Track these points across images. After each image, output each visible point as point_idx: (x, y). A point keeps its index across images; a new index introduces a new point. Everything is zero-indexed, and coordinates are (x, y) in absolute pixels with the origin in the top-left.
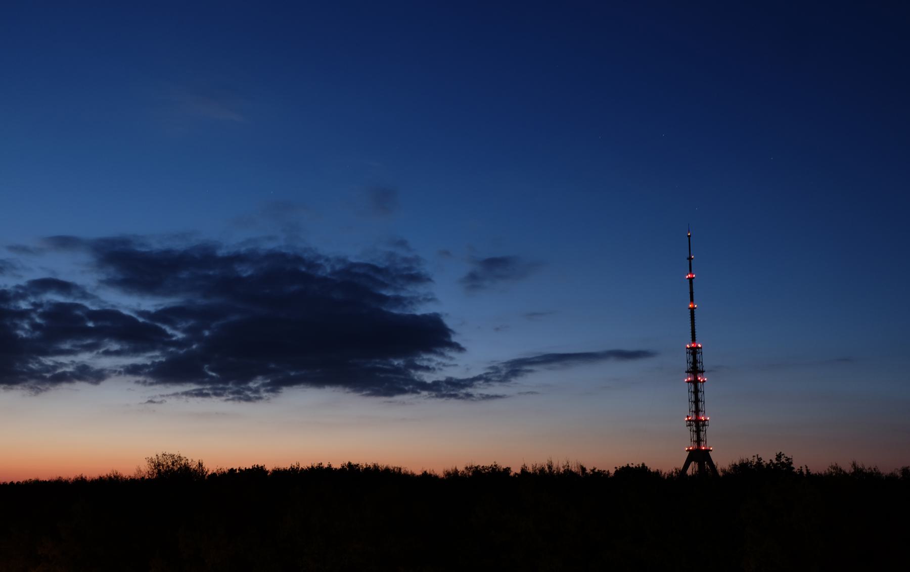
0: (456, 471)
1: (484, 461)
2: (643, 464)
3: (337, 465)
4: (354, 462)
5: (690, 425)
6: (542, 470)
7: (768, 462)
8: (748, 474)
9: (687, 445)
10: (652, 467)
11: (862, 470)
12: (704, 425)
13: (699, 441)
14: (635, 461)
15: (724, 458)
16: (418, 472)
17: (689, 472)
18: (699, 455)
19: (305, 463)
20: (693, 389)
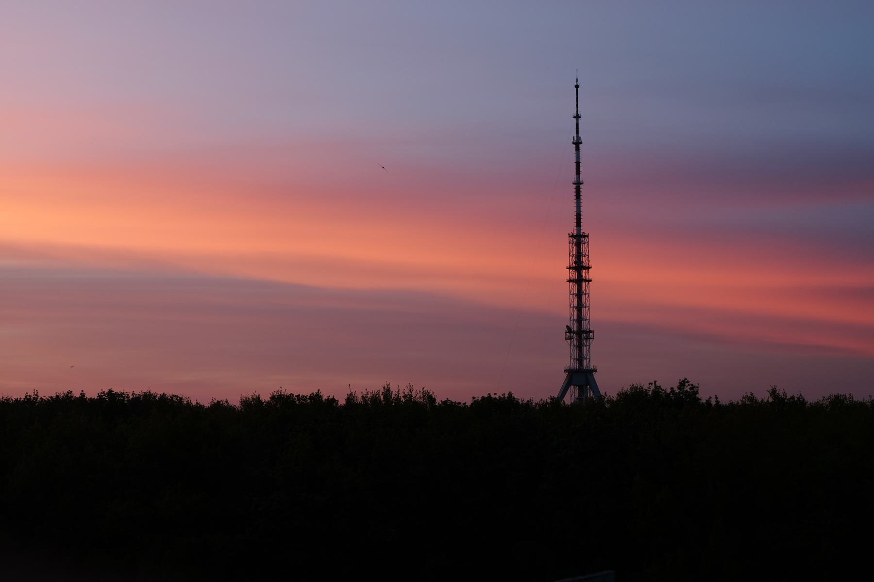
0: (258, 399)
1: (132, 383)
2: (510, 394)
3: (92, 393)
4: (117, 390)
5: (570, 338)
6: (375, 399)
7: (669, 391)
8: (638, 401)
9: (563, 358)
10: (522, 396)
11: (783, 400)
12: (588, 338)
13: (580, 359)
14: (498, 390)
15: (611, 382)
16: (736, 397)
17: (568, 400)
18: (580, 376)
19: (47, 390)
20: (575, 291)
